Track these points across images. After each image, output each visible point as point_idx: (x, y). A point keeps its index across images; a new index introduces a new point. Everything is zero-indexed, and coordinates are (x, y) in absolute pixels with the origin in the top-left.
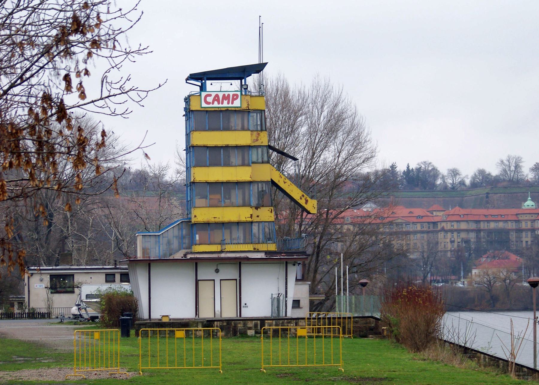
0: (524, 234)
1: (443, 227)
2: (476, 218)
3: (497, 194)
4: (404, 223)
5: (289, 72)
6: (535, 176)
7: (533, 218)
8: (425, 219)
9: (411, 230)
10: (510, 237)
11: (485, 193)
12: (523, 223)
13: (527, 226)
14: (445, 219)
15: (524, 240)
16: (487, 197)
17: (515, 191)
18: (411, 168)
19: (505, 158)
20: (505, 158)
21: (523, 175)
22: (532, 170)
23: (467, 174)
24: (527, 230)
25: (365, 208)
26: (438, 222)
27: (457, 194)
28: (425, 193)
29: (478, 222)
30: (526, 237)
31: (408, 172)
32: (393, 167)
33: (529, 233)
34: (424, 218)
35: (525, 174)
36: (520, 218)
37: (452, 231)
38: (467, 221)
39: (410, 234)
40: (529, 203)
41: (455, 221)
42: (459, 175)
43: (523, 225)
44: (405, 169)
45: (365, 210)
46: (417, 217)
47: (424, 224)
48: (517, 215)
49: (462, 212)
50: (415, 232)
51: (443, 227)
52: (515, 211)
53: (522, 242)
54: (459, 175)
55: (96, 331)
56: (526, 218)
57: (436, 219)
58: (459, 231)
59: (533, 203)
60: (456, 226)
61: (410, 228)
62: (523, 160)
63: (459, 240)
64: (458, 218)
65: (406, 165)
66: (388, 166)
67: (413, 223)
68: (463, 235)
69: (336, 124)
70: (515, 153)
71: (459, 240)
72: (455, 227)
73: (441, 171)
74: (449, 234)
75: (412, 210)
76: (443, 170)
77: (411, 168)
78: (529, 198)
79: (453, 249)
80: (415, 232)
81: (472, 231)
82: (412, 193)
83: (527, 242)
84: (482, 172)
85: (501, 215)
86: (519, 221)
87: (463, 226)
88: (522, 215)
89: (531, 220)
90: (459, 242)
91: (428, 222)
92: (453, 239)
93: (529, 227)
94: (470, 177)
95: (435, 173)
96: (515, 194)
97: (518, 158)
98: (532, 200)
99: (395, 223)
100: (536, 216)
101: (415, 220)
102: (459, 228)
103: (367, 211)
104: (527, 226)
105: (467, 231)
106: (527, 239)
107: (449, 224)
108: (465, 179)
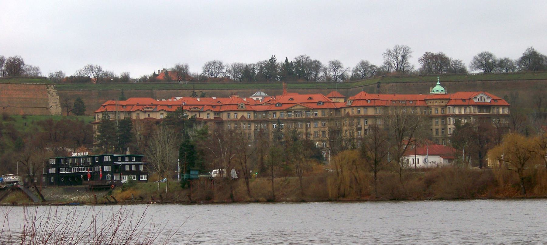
0: (434, 121)
1: (348, 113)
2: (384, 103)
3: (389, 83)
4: (303, 109)
5: (63, 72)
6: (424, 67)
7: (444, 104)
8: (325, 106)
9: (312, 117)
11: (376, 82)
12: (433, 109)
14: (350, 104)
15: (434, 127)
16: (378, 87)
17: (407, 80)
18: (289, 61)
19: (392, 48)
20: (392, 48)
21: (409, 66)
22: (421, 60)
23: (349, 66)
24: (437, 117)
25: (255, 96)
26: (341, 108)
27: (345, 85)
28: (309, 85)
29: (385, 107)
30: (437, 124)
31: (287, 65)
32: (272, 60)
33: (440, 121)
34: (325, 104)
36: (429, 104)
37: (359, 117)
38: (374, 107)
39: (310, 122)
40: (438, 88)
41: (362, 106)
42: (341, 67)
43: (433, 112)
44: (284, 62)
45: (255, 98)
46: (317, 103)
48: (425, 100)
49: (369, 96)
50: (316, 120)
51: (348, 113)
52: (422, 97)
53: (432, 130)
54: (341, 67)
55: (141, 164)
56: (437, 104)
57: (338, 106)
58: (366, 117)
61: (311, 115)
62: (411, 50)
63: (366, 127)
64: (365, 104)
65: (285, 59)
66: (267, 58)
67: (314, 109)
68: (370, 122)
70: (402, 43)
71: (366, 127)
72: (362, 113)
73: (323, 64)
76: (325, 63)
77: (289, 61)
78: (438, 83)
79: (360, 137)
80: (316, 120)
81: (380, 117)
82: (296, 85)
83: (437, 130)
84: (364, 65)
86: (428, 107)
87: (371, 112)
88: (432, 101)
89: (441, 106)
90: (366, 130)
91: (330, 109)
92: (359, 126)
93: (440, 113)
94: (351, 69)
95: (316, 66)
96: (408, 84)
97: (406, 48)
98: (441, 85)
99: (294, 110)
100: (447, 101)
101: (315, 106)
102: (366, 114)
103: (258, 100)
106: (437, 127)
107: (355, 110)
108: (347, 72)
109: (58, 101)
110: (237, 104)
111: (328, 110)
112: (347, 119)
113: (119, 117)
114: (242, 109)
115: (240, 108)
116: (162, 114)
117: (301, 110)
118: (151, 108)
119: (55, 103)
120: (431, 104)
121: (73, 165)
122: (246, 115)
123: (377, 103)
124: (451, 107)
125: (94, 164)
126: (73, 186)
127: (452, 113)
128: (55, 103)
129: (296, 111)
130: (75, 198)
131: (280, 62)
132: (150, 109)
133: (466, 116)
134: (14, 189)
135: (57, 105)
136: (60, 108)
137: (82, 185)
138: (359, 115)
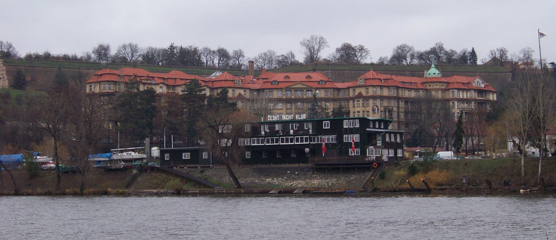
4: (305, 88)
7: (443, 87)
10: (4, 68)
13: (453, 96)
17: (341, 68)
35: (123, 69)
36: (428, 87)
37: (374, 98)
38: (388, 87)
47: (330, 90)
54: (243, 56)
56: (437, 87)
58: (382, 98)
59: (437, 72)
60: (378, 92)
69: (124, 47)
74: (371, 102)
75: (290, 75)
85: (412, 83)
87: (386, 92)
88: (438, 84)
99: (294, 88)
104: (453, 96)
105: (389, 98)
109: (4, 72)
110: (233, 81)
111: (332, 90)
112: (361, 101)
113: (91, 89)
114: (239, 86)
115: (237, 85)
116: (161, 87)
117: (301, 90)
118: (150, 80)
119: (2, 74)
120: (431, 87)
121: (273, 133)
122: (242, 92)
123: (390, 83)
124: (456, 91)
125: (319, 130)
126: (272, 165)
127: (456, 96)
128: (2, 74)
129: (296, 90)
130: (155, 191)
131: (202, 48)
132: (148, 82)
133: (468, 101)
134: (146, 170)
135: (3, 78)
136: (7, 81)
137: (308, 163)
138: (368, 95)
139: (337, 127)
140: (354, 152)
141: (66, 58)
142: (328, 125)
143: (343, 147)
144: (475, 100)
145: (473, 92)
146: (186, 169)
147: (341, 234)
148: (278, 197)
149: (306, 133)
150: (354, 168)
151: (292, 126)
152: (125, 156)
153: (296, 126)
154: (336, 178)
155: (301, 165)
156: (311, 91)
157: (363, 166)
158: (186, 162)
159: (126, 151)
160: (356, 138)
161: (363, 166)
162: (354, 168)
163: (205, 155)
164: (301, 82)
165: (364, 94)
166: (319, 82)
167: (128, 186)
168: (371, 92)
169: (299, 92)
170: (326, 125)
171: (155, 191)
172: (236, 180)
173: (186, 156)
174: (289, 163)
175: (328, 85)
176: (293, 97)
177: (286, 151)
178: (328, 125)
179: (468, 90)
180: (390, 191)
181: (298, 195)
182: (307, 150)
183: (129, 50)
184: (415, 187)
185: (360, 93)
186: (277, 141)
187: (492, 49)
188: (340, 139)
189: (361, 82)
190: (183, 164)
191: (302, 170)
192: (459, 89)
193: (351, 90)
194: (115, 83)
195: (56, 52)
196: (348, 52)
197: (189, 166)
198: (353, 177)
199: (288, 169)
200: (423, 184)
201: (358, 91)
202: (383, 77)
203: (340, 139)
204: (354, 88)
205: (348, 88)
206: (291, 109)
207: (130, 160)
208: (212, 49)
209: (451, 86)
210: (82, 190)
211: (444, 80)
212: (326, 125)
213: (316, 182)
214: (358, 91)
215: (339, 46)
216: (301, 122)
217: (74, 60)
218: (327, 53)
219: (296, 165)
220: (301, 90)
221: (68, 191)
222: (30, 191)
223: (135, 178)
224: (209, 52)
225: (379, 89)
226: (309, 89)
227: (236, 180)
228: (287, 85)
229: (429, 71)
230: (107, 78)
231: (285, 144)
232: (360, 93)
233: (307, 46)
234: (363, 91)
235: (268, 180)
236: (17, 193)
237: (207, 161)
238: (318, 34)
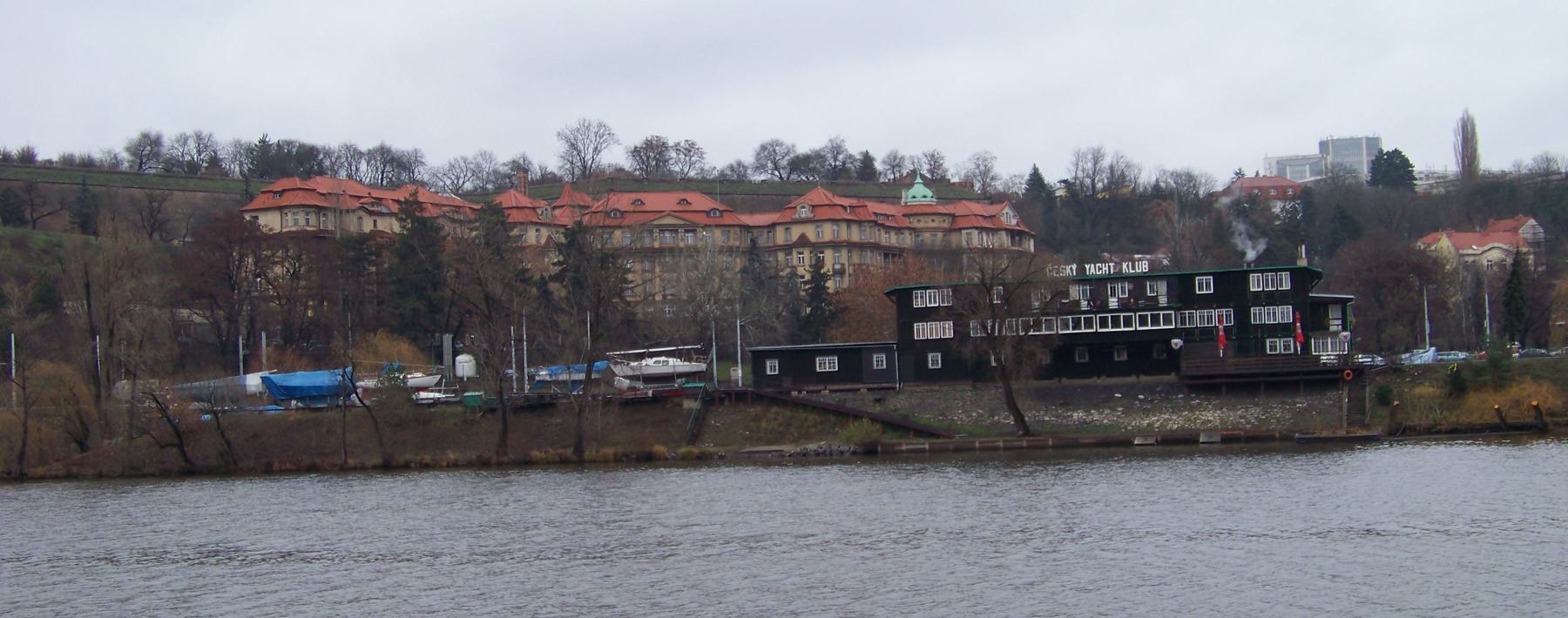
7: (946, 225)
36: (916, 225)
38: (859, 223)
54: (422, 163)
58: (851, 246)
60: (844, 233)
87: (855, 235)
105: (861, 246)
112: (807, 254)
117: (674, 229)
124: (975, 232)
129: (663, 229)
139: (1231, 288)
140: (1278, 346)
141: (68, 162)
142: (1208, 285)
143: (1247, 336)
144: (1009, 252)
145: (1004, 234)
146: (827, 395)
147: (1059, 556)
148: (1222, 453)
149: (1153, 304)
150: (1296, 383)
151: (1113, 290)
152: (652, 365)
153: (1122, 291)
154: (1257, 405)
155: (1143, 378)
156: (694, 231)
157: (1309, 378)
158: (827, 378)
159: (652, 355)
160: (1283, 314)
161: (1309, 378)
162: (1296, 383)
163: (879, 361)
164: (673, 213)
165: (812, 237)
166: (707, 213)
167: (694, 438)
168: (828, 232)
169: (667, 235)
170: (1205, 286)
171: (788, 448)
172: (1019, 417)
173: (827, 364)
174: (1108, 376)
175: (727, 219)
176: (657, 245)
177: (1100, 347)
178: (1208, 285)
179: (994, 231)
180: (1099, 444)
181: (1209, 451)
182: (1177, 343)
183: (192, 145)
184: (1509, 421)
185: (803, 237)
186: (1077, 325)
187: (902, 152)
188: (1242, 316)
189: (804, 213)
190: (818, 383)
191: (1149, 389)
192: (981, 229)
193: (780, 231)
194: (319, 209)
195: (48, 151)
196: (652, 152)
197: (811, 388)
198: (1301, 403)
199: (1117, 388)
200: (1532, 412)
201: (796, 232)
202: (846, 202)
203: (1242, 316)
204: (788, 225)
205: (773, 226)
206: (653, 271)
207: (668, 378)
208: (364, 148)
209: (961, 223)
210: (579, 449)
211: (942, 209)
212: (1205, 286)
213: (1211, 416)
214: (796, 232)
215: (638, 141)
216: (1138, 281)
217: (88, 165)
218: (615, 157)
219: (1132, 379)
220: (674, 229)
221: (536, 454)
222: (428, 459)
223: (700, 419)
224: (354, 154)
225: (844, 226)
226: (691, 228)
227: (1019, 417)
228: (642, 218)
229: (912, 192)
230: (300, 198)
231: (1044, 332)
232: (803, 237)
233: (568, 140)
234: (810, 232)
235: (1078, 415)
236: (388, 467)
237: (887, 374)
238: (594, 115)
